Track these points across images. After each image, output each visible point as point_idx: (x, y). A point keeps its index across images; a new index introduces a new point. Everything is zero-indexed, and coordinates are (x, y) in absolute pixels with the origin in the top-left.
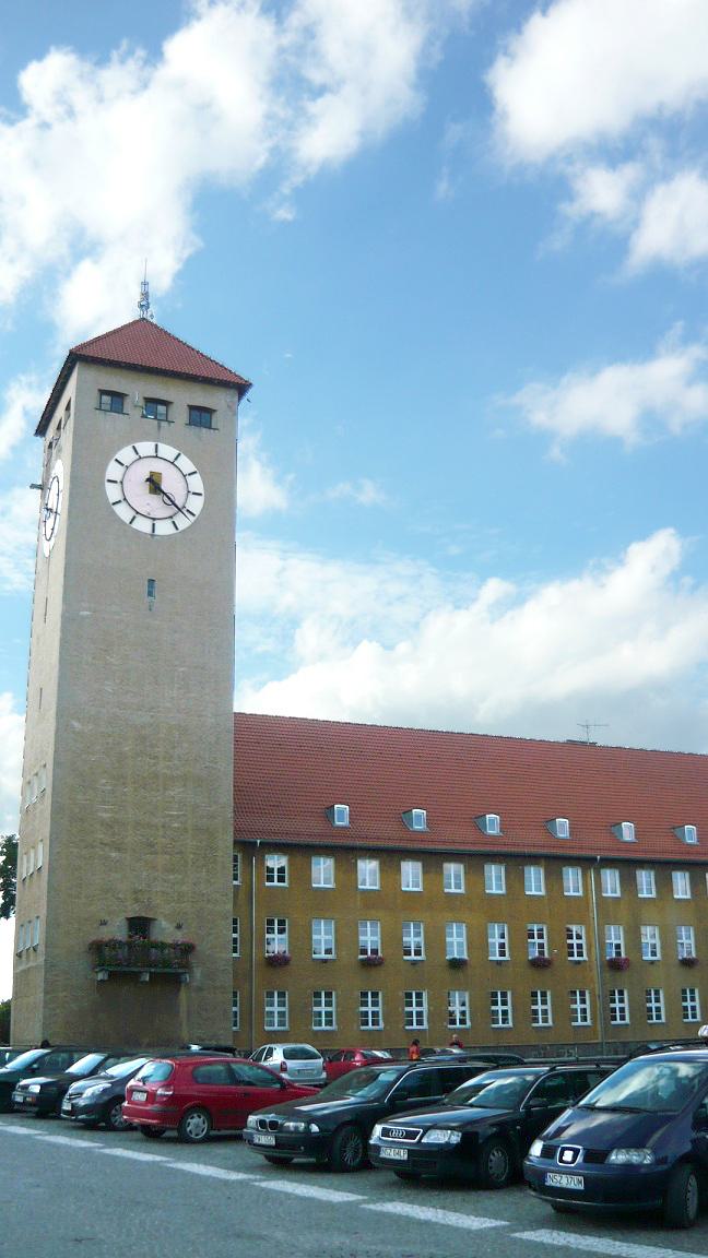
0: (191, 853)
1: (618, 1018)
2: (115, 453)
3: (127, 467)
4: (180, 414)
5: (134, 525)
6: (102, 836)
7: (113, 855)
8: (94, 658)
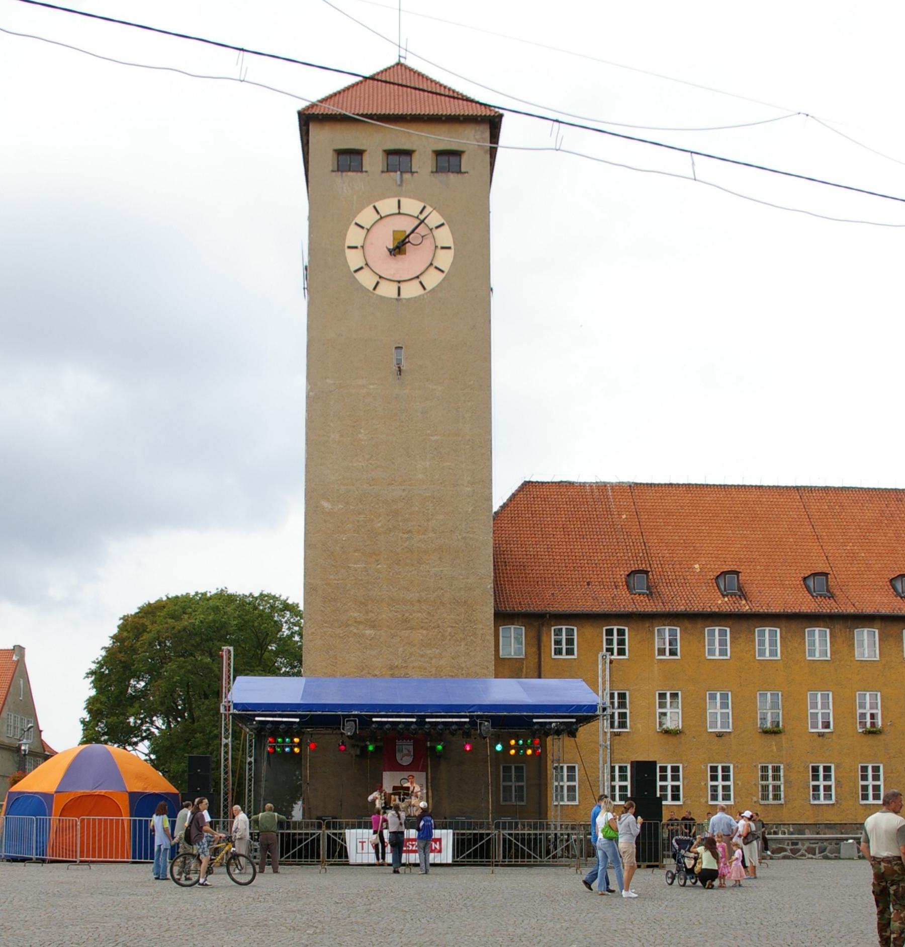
0: (449, 626)
1: (720, 797)
2: (377, 201)
3: (368, 230)
4: (423, 162)
5: (379, 291)
6: (356, 614)
7: (368, 632)
8: (341, 436)
